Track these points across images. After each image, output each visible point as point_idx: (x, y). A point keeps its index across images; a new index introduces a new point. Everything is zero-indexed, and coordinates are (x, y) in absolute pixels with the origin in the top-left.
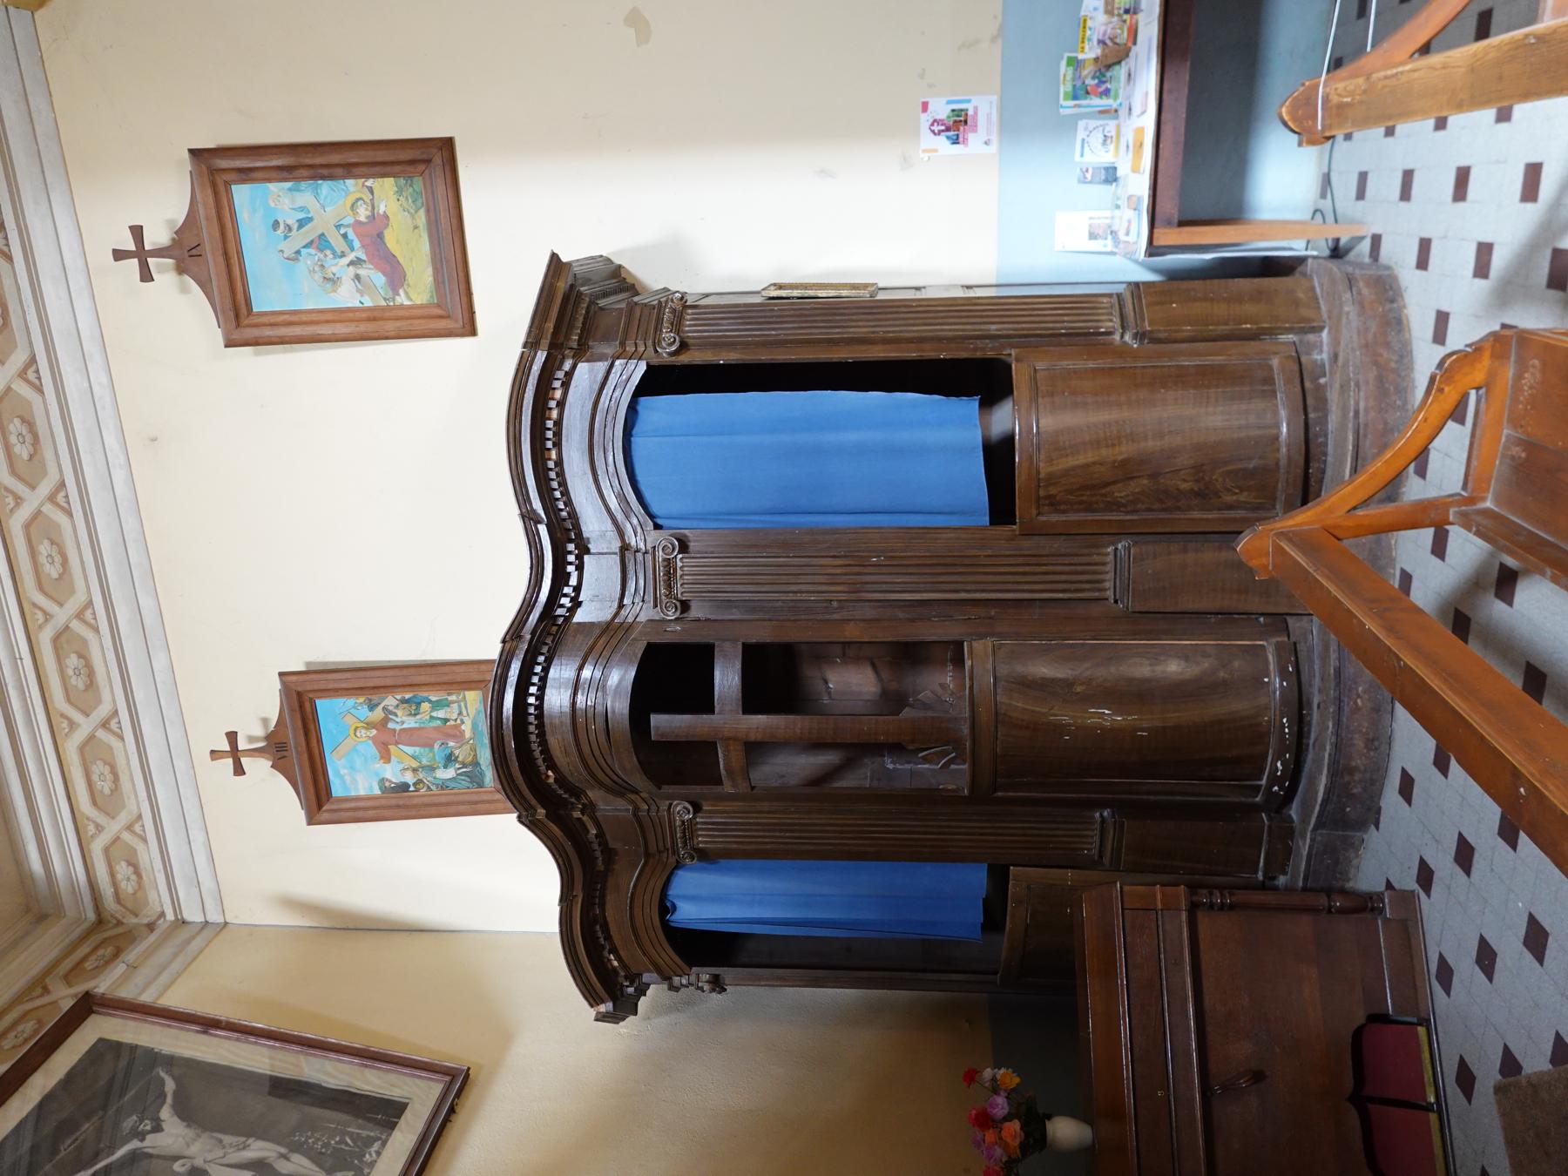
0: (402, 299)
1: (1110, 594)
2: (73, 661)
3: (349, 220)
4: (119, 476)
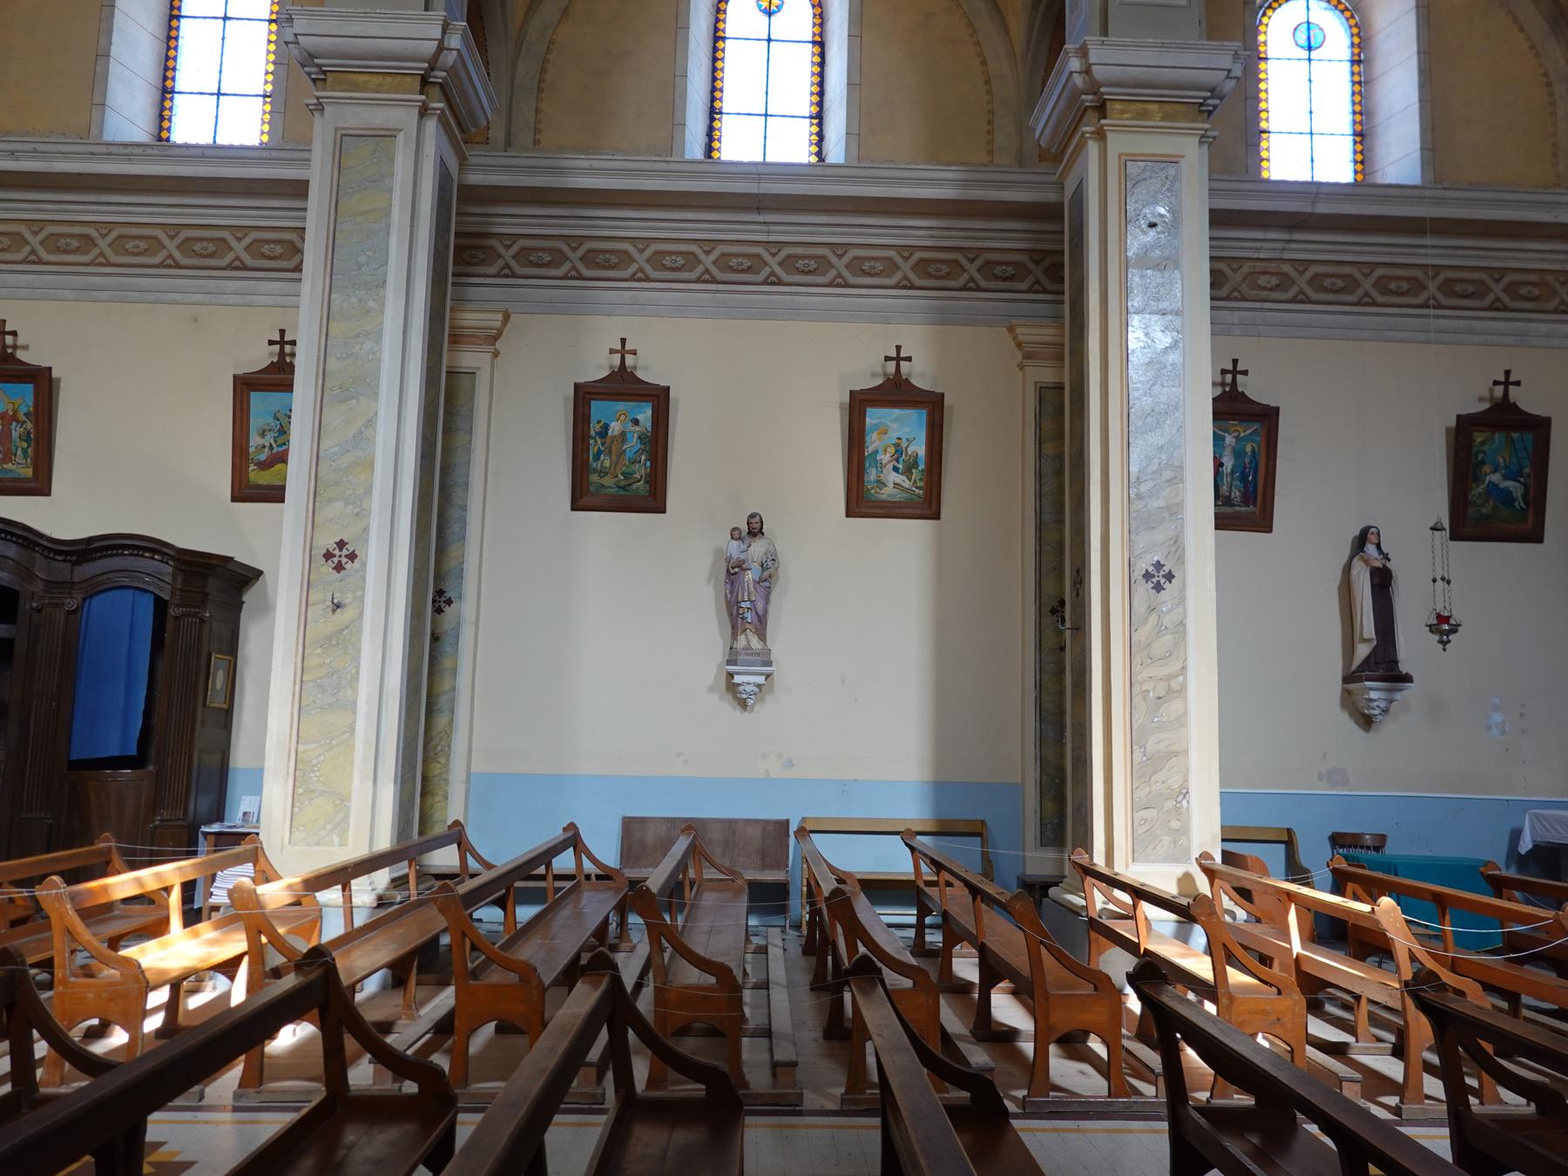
0: (252, 467)
1: (24, 816)
2: (75, 244)
4: (178, 297)
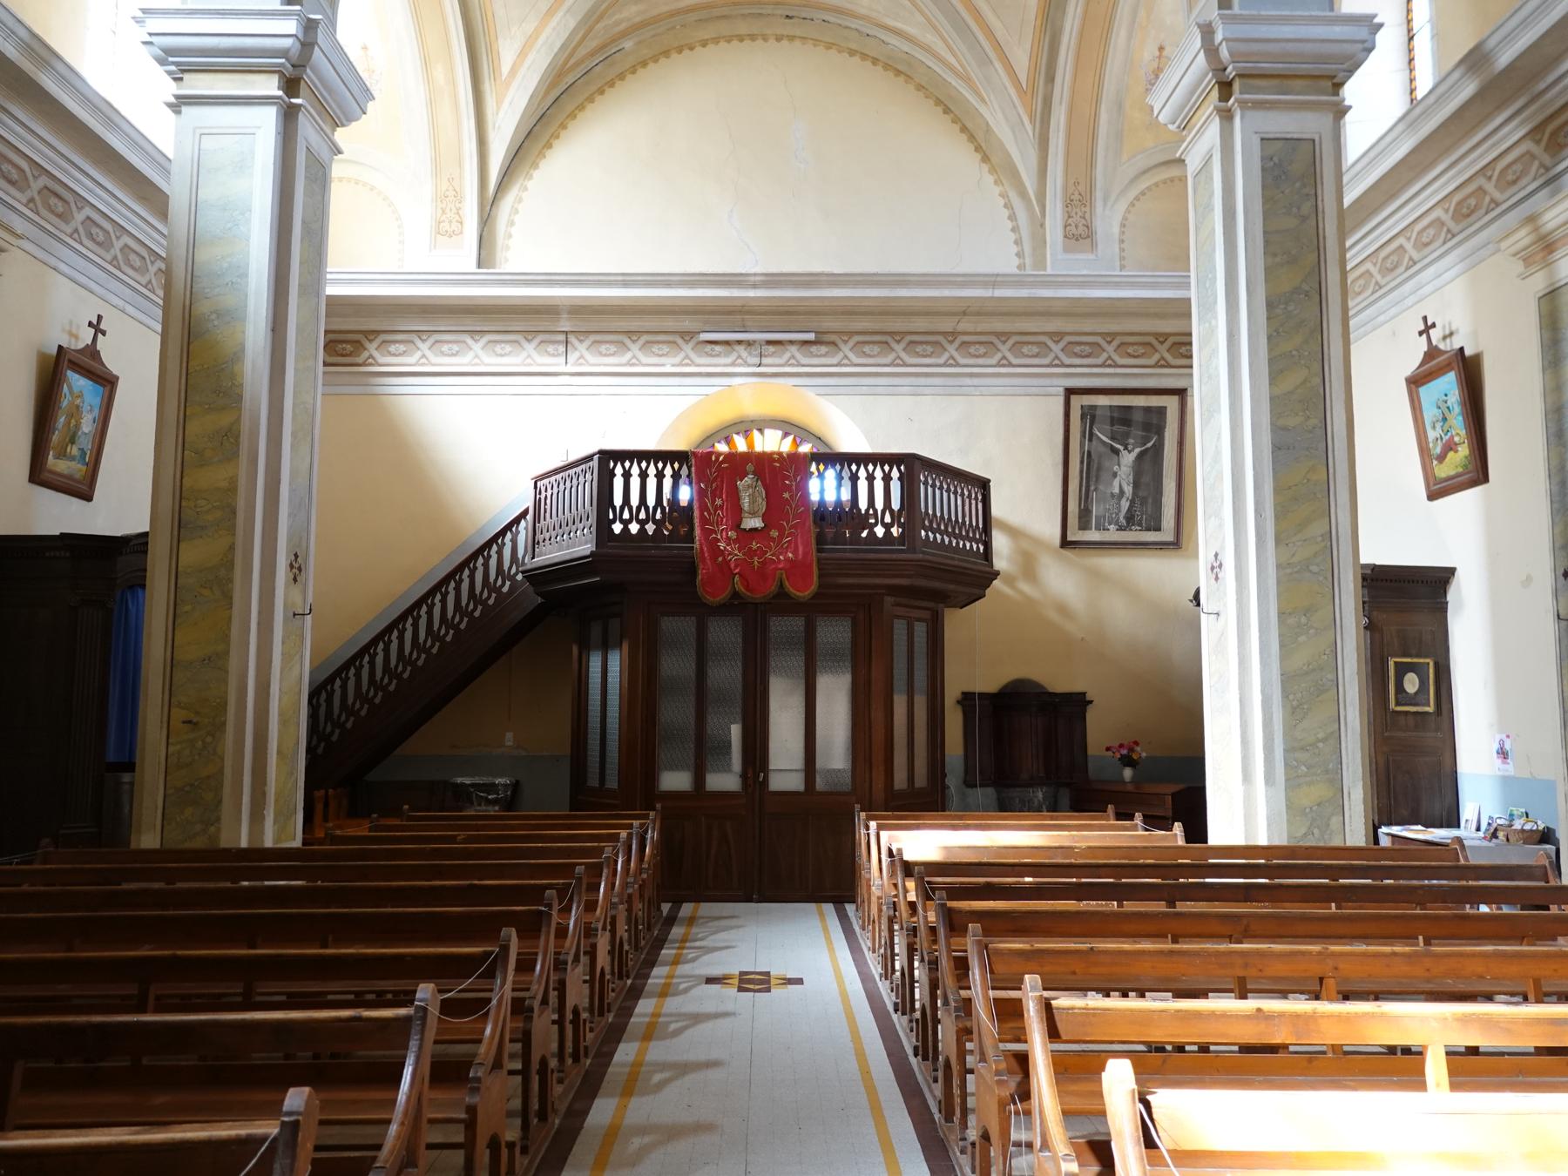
3: (1454, 433)
